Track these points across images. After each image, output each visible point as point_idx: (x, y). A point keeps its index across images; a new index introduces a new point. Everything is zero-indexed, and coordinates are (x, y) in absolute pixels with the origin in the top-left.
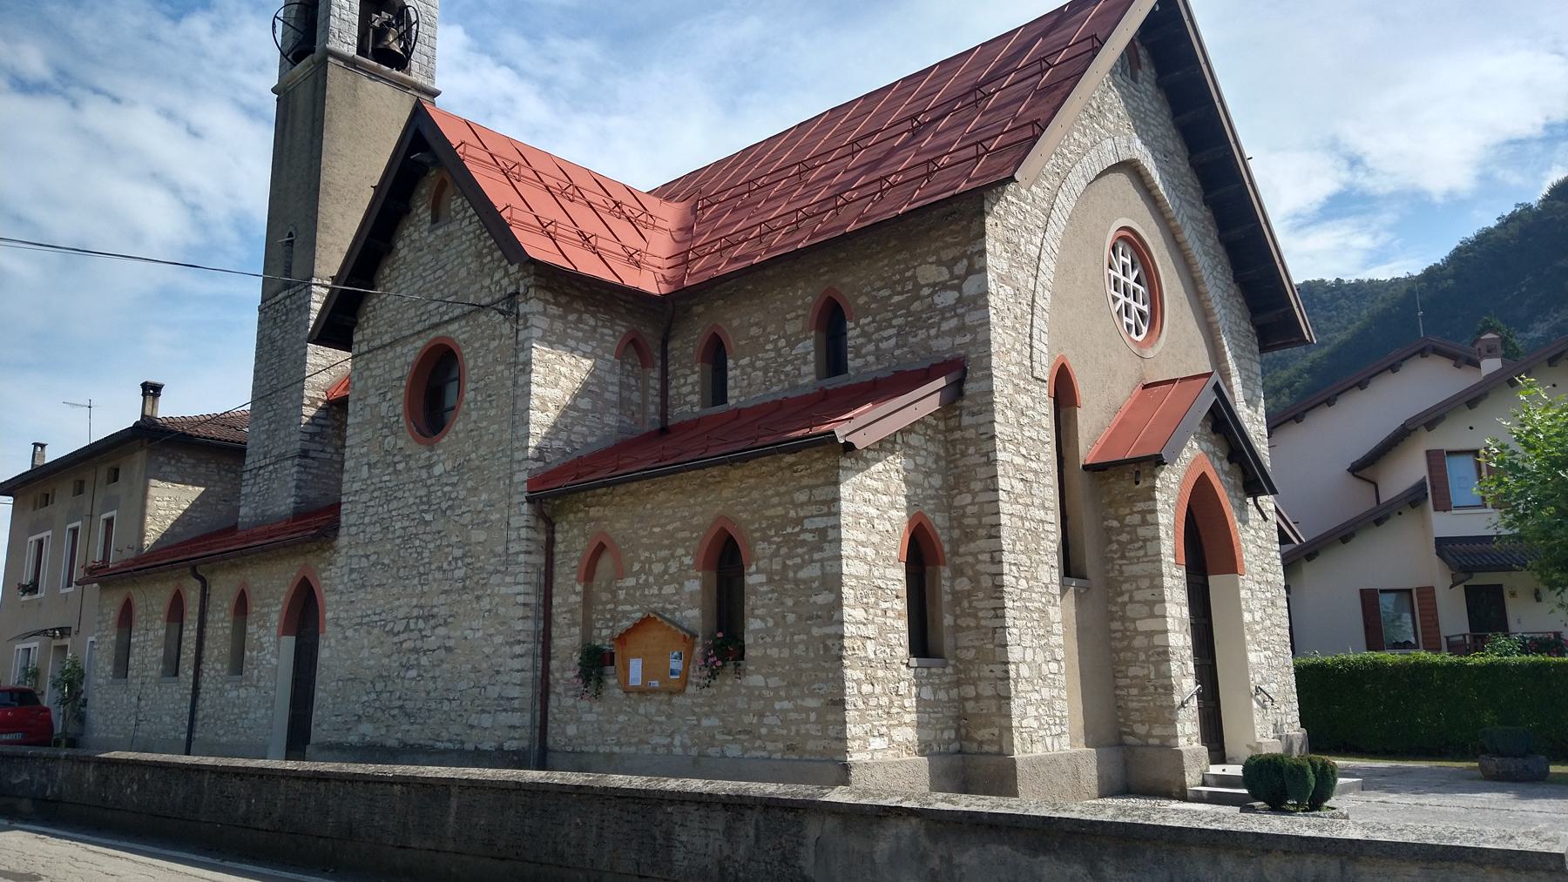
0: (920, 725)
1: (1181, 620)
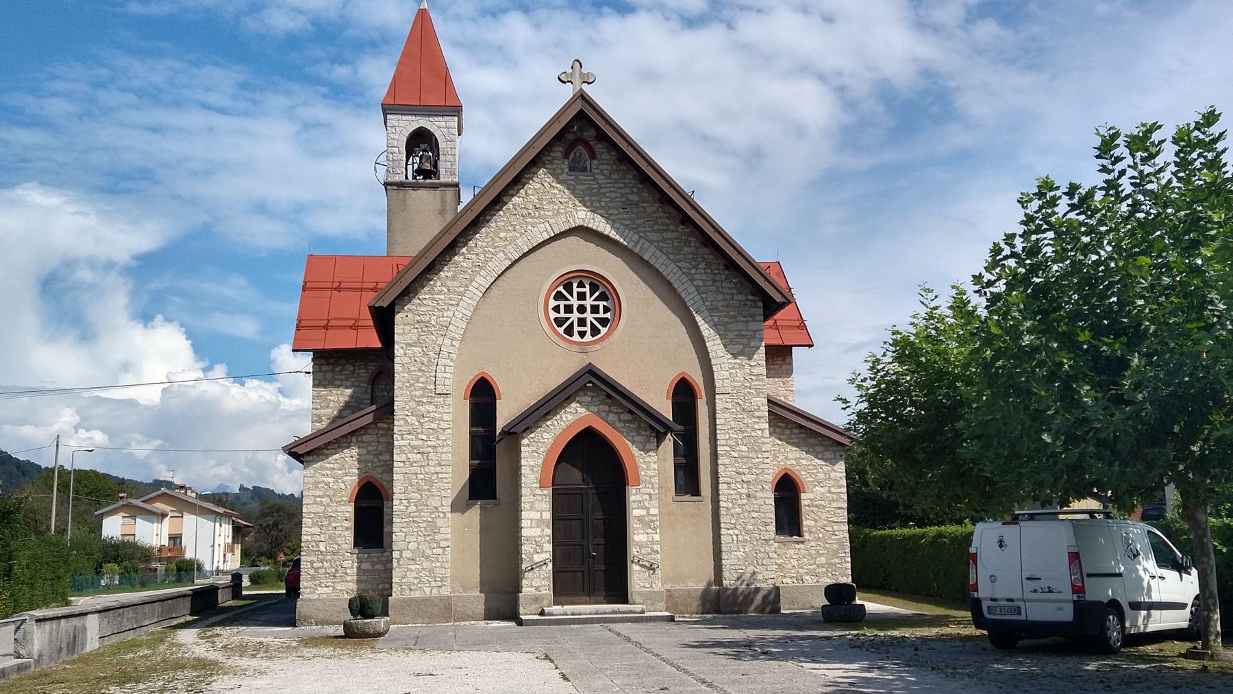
0: (358, 582)
1: (540, 521)
